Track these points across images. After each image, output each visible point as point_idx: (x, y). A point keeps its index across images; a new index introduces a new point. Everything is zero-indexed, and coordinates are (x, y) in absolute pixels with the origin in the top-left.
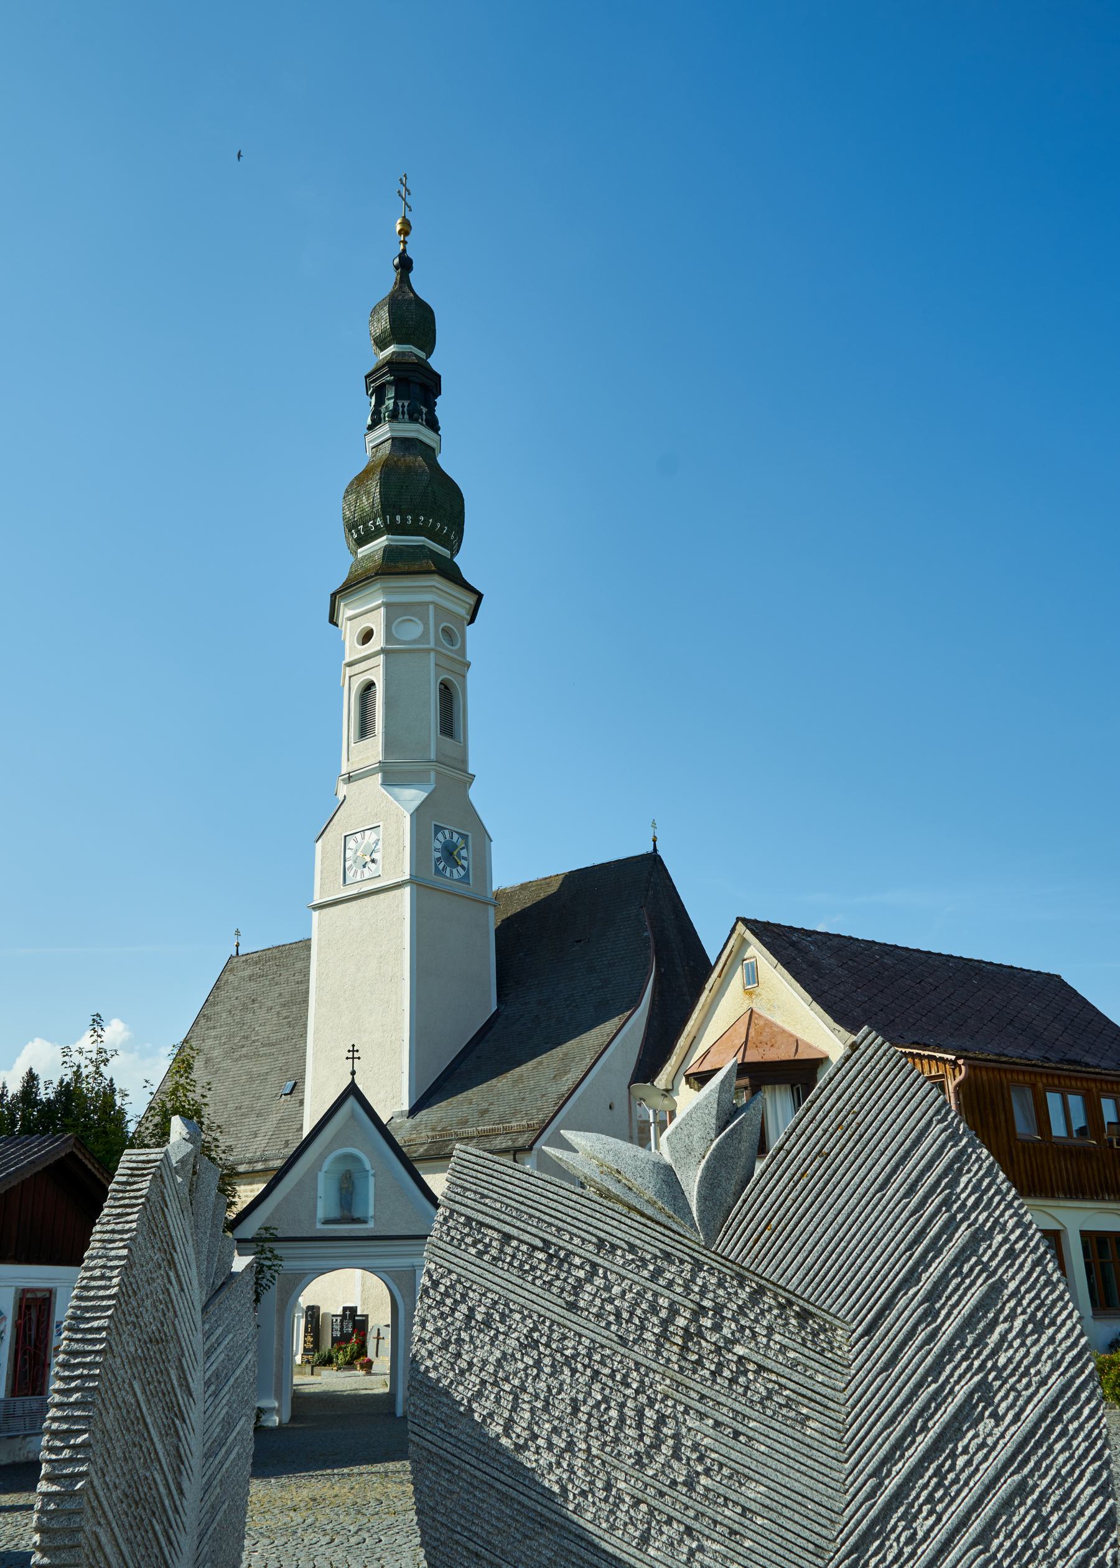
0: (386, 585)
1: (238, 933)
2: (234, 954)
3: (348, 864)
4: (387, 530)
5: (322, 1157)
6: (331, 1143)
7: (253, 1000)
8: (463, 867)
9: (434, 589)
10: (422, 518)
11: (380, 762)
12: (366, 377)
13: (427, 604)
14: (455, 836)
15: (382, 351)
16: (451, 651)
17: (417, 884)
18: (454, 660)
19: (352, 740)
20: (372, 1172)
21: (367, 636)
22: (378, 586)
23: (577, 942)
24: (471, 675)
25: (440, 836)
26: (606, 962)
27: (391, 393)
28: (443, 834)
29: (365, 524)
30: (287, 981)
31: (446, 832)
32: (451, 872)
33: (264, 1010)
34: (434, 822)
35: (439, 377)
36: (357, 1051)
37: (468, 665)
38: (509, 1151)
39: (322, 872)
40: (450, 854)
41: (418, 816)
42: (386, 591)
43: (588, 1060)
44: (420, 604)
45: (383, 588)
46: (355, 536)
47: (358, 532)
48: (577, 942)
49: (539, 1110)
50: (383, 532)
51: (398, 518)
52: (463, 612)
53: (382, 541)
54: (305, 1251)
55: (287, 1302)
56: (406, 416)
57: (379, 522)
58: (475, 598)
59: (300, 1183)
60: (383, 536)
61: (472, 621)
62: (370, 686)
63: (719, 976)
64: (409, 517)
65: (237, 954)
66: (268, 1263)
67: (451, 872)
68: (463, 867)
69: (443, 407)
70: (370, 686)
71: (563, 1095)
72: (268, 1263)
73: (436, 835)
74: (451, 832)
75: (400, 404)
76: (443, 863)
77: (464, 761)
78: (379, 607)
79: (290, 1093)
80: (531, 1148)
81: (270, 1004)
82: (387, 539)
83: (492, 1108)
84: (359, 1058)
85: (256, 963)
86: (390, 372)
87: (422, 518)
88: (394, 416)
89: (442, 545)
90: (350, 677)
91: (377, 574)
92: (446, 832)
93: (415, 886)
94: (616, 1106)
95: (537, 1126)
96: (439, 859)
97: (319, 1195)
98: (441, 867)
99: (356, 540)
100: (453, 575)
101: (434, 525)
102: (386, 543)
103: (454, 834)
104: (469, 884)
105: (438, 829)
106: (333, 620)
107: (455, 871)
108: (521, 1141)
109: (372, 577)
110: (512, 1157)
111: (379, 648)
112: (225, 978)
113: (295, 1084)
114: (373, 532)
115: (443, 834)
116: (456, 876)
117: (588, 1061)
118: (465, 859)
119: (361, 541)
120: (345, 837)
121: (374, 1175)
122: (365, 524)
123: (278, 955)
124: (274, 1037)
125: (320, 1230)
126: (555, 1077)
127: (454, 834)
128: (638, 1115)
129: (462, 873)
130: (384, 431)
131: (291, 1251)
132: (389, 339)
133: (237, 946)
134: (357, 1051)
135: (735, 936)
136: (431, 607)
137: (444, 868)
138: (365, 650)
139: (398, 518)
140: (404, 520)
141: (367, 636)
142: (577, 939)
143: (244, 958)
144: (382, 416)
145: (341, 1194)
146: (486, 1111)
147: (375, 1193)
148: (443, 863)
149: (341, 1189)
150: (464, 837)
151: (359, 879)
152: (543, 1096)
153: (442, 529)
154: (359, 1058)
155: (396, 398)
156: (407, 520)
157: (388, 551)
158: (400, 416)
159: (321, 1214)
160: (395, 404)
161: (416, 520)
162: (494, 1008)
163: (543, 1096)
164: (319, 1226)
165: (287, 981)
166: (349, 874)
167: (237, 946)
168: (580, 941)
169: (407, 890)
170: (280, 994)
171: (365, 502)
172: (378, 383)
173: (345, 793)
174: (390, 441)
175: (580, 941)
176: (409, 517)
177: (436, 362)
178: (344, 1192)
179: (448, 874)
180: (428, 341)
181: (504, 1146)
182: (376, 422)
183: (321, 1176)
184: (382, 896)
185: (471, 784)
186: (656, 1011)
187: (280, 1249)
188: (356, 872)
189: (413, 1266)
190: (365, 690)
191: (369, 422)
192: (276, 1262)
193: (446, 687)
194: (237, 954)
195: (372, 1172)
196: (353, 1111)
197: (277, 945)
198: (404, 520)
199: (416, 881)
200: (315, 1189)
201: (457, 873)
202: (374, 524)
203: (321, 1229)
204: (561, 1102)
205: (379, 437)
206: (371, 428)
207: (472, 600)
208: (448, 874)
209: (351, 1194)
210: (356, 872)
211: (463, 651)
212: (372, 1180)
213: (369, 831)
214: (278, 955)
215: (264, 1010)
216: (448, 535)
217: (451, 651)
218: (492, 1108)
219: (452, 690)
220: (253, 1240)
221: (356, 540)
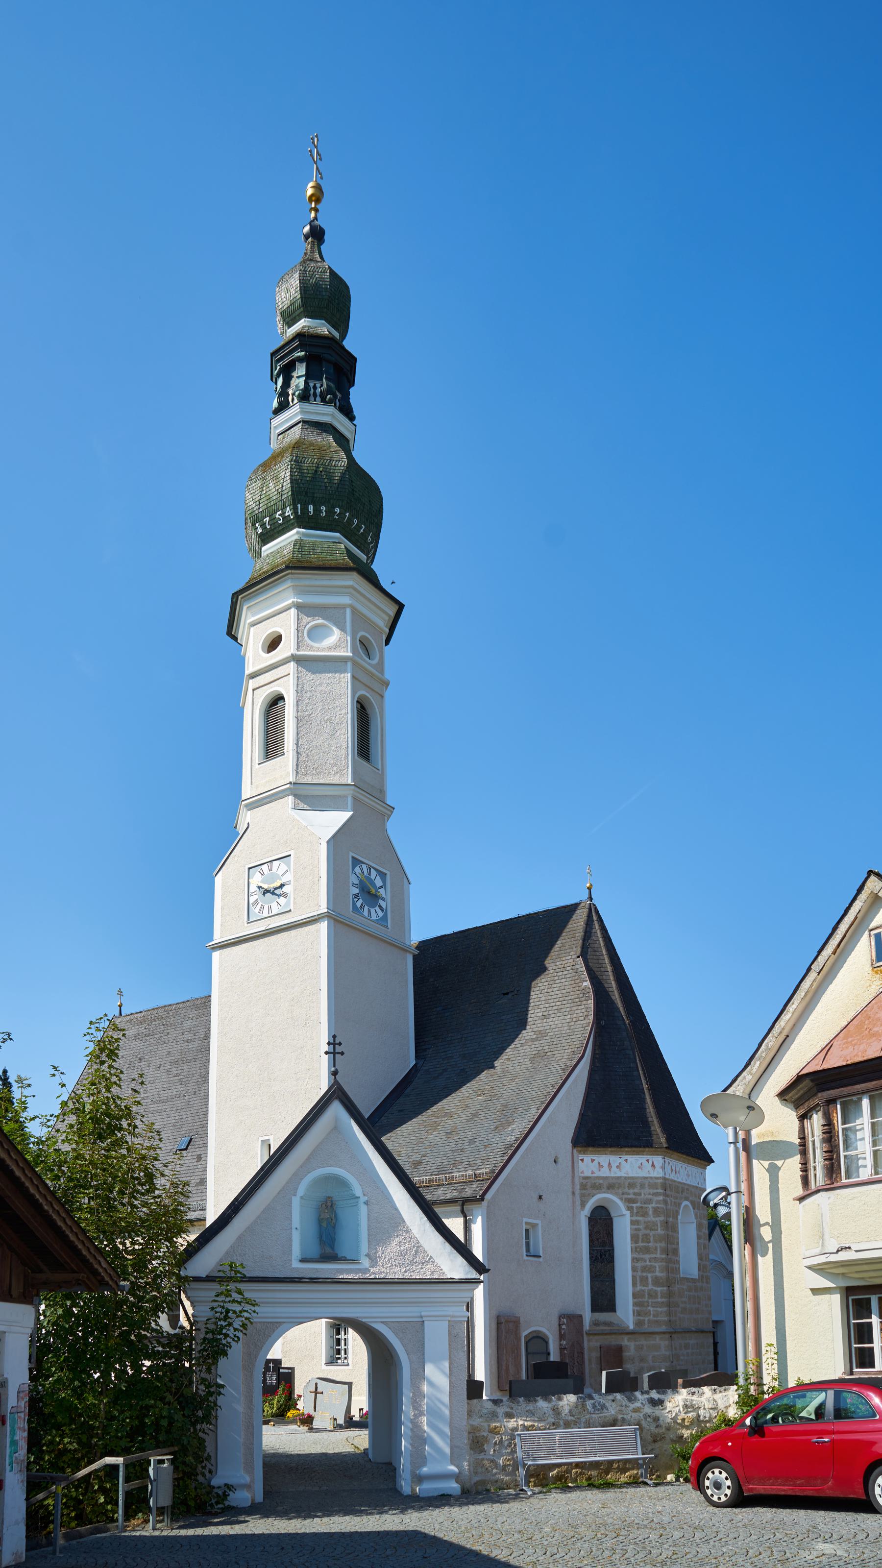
0: (297, 583)
1: (120, 993)
2: (117, 1014)
3: (252, 900)
4: (297, 522)
5: (297, 1177)
6: (308, 1159)
7: (140, 1059)
8: (380, 907)
9: (351, 590)
10: (338, 510)
11: (290, 783)
12: (273, 354)
13: (343, 607)
14: (374, 873)
15: (289, 327)
16: (369, 664)
17: (335, 920)
18: (372, 675)
19: (256, 761)
20: (363, 1199)
21: (274, 643)
22: (288, 584)
23: (504, 994)
24: (388, 694)
25: (357, 869)
26: (540, 1014)
27: (301, 370)
28: (361, 868)
29: (271, 515)
30: (176, 1040)
31: (364, 866)
32: (369, 912)
33: (153, 1068)
34: (351, 854)
35: (355, 359)
36: (340, 1044)
37: (386, 684)
38: (456, 1202)
39: (222, 908)
40: (369, 895)
41: (336, 842)
42: (299, 591)
43: (534, 1110)
44: (336, 607)
45: (294, 587)
46: (260, 531)
47: (263, 525)
48: (504, 994)
49: (484, 1161)
50: (292, 524)
51: (311, 508)
52: (383, 625)
53: (293, 535)
54: (278, 1295)
55: (256, 1357)
56: (318, 399)
57: (288, 512)
58: (395, 608)
59: (268, 1209)
60: (292, 529)
61: (387, 642)
62: (277, 700)
63: (834, 953)
64: (324, 508)
65: (121, 1014)
66: (238, 1308)
67: (369, 912)
68: (380, 907)
69: (356, 395)
70: (277, 700)
71: (511, 1145)
72: (238, 1308)
73: (353, 869)
74: (369, 868)
75: (312, 385)
76: (360, 901)
77: (382, 791)
78: (290, 608)
79: (186, 1149)
80: (482, 1198)
81: (158, 1062)
82: (298, 533)
83: (426, 1159)
84: (342, 1053)
85: (141, 1023)
86: (301, 347)
87: (338, 510)
88: (304, 397)
89: (358, 548)
90: (254, 690)
91: (288, 567)
92: (364, 866)
93: (332, 921)
94: (560, 1160)
95: (485, 1177)
96: (356, 896)
97: (294, 1226)
98: (359, 904)
99: (260, 536)
100: (372, 579)
101: (350, 521)
102: (296, 537)
103: (372, 870)
104: (387, 927)
105: (356, 862)
106: (231, 633)
107: (372, 910)
108: (469, 1192)
109: (281, 571)
110: (458, 1208)
111: (289, 654)
112: (303, 750)
113: (191, 1139)
114: (281, 524)
115: (361, 868)
116: (374, 917)
117: (534, 1112)
118: (384, 900)
119: (266, 537)
120: (249, 869)
121: (366, 1203)
122: (271, 515)
123: (164, 1014)
124: (165, 1094)
125: (297, 1269)
126: (496, 1128)
127: (372, 870)
128: (580, 1171)
129: (381, 914)
130: (295, 412)
131: (270, 1295)
132: (299, 312)
133: (120, 1006)
134: (340, 1044)
135: (863, 896)
136: (348, 611)
137: (362, 906)
138: (271, 658)
139: (311, 508)
140: (317, 510)
141: (274, 643)
142: (505, 992)
143: (128, 1018)
144: (290, 398)
145: (320, 1226)
146: (419, 1163)
147: (369, 1226)
148: (360, 901)
149: (320, 1221)
150: (383, 875)
151: (265, 914)
152: (486, 1146)
153: (359, 527)
154: (342, 1053)
155: (308, 376)
156: (321, 511)
157: (299, 545)
158: (312, 398)
159: (296, 1251)
160: (306, 382)
161: (331, 512)
162: (413, 1063)
163: (486, 1146)
164: (296, 1264)
165: (176, 1040)
166: (255, 910)
167: (120, 1006)
168: (507, 994)
169: (324, 926)
170: (169, 1053)
171: (272, 488)
172: (286, 361)
173: (248, 820)
174: (300, 425)
175: (507, 994)
176: (324, 508)
177: (348, 344)
178: (324, 1224)
179: (366, 913)
180: (340, 319)
181: (448, 1196)
182: (283, 406)
183: (296, 1202)
184: (293, 933)
185: (389, 816)
186: (598, 1065)
187: (251, 1291)
188: (262, 907)
189: (422, 1317)
190: (271, 706)
191: (275, 404)
192: (248, 1307)
193: (362, 707)
194: (121, 1014)
195: (363, 1199)
196: (337, 1120)
197: (163, 1004)
198: (317, 510)
199: (334, 917)
200: (289, 1218)
201: (376, 914)
202: (282, 514)
203: (297, 1267)
204: (510, 1152)
205: (287, 421)
206: (277, 412)
207: (392, 610)
208: (366, 913)
209: (334, 1227)
210: (262, 907)
211: (380, 666)
212: (363, 1210)
213: (277, 862)
214: (164, 1014)
215: (153, 1068)
216: (365, 535)
217: (369, 664)
218: (426, 1159)
219: (369, 711)
220: (209, 1279)
221: (260, 536)
